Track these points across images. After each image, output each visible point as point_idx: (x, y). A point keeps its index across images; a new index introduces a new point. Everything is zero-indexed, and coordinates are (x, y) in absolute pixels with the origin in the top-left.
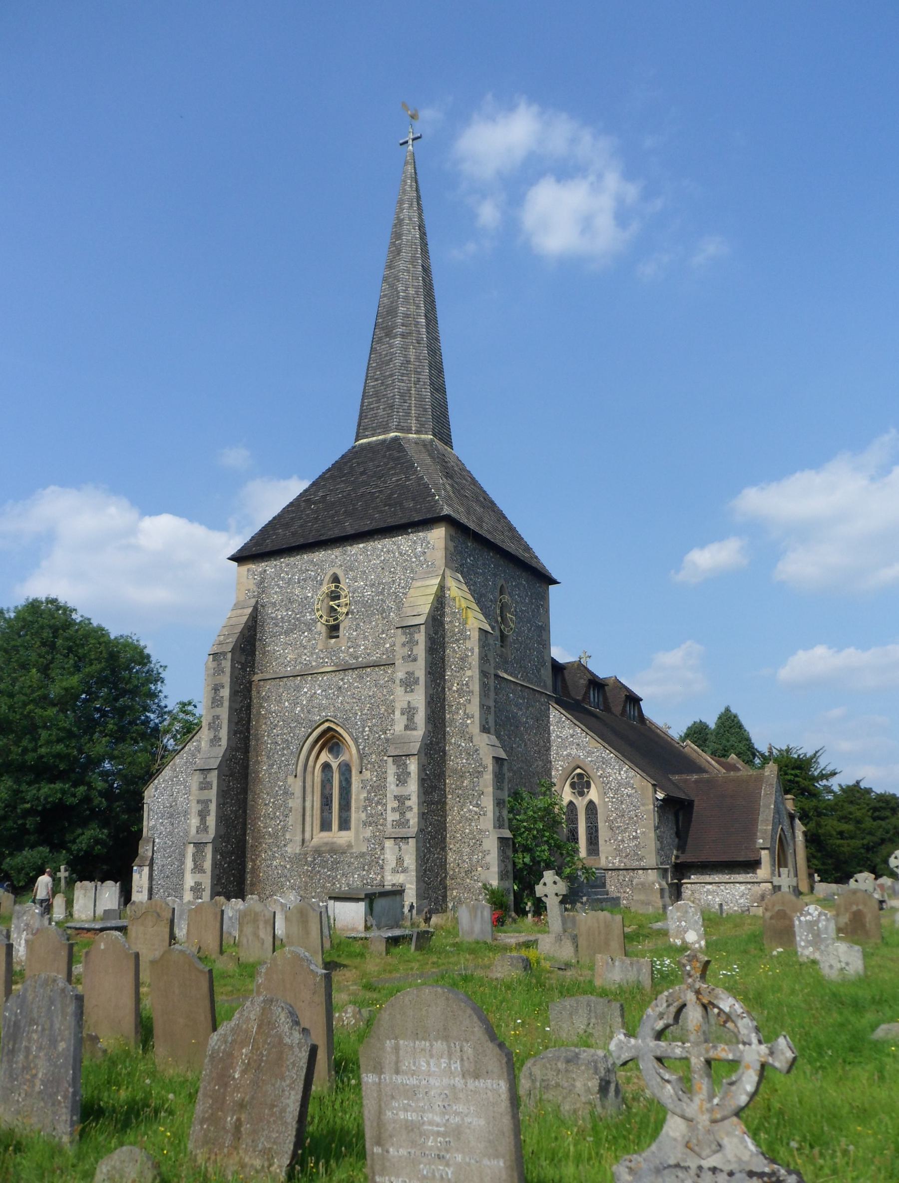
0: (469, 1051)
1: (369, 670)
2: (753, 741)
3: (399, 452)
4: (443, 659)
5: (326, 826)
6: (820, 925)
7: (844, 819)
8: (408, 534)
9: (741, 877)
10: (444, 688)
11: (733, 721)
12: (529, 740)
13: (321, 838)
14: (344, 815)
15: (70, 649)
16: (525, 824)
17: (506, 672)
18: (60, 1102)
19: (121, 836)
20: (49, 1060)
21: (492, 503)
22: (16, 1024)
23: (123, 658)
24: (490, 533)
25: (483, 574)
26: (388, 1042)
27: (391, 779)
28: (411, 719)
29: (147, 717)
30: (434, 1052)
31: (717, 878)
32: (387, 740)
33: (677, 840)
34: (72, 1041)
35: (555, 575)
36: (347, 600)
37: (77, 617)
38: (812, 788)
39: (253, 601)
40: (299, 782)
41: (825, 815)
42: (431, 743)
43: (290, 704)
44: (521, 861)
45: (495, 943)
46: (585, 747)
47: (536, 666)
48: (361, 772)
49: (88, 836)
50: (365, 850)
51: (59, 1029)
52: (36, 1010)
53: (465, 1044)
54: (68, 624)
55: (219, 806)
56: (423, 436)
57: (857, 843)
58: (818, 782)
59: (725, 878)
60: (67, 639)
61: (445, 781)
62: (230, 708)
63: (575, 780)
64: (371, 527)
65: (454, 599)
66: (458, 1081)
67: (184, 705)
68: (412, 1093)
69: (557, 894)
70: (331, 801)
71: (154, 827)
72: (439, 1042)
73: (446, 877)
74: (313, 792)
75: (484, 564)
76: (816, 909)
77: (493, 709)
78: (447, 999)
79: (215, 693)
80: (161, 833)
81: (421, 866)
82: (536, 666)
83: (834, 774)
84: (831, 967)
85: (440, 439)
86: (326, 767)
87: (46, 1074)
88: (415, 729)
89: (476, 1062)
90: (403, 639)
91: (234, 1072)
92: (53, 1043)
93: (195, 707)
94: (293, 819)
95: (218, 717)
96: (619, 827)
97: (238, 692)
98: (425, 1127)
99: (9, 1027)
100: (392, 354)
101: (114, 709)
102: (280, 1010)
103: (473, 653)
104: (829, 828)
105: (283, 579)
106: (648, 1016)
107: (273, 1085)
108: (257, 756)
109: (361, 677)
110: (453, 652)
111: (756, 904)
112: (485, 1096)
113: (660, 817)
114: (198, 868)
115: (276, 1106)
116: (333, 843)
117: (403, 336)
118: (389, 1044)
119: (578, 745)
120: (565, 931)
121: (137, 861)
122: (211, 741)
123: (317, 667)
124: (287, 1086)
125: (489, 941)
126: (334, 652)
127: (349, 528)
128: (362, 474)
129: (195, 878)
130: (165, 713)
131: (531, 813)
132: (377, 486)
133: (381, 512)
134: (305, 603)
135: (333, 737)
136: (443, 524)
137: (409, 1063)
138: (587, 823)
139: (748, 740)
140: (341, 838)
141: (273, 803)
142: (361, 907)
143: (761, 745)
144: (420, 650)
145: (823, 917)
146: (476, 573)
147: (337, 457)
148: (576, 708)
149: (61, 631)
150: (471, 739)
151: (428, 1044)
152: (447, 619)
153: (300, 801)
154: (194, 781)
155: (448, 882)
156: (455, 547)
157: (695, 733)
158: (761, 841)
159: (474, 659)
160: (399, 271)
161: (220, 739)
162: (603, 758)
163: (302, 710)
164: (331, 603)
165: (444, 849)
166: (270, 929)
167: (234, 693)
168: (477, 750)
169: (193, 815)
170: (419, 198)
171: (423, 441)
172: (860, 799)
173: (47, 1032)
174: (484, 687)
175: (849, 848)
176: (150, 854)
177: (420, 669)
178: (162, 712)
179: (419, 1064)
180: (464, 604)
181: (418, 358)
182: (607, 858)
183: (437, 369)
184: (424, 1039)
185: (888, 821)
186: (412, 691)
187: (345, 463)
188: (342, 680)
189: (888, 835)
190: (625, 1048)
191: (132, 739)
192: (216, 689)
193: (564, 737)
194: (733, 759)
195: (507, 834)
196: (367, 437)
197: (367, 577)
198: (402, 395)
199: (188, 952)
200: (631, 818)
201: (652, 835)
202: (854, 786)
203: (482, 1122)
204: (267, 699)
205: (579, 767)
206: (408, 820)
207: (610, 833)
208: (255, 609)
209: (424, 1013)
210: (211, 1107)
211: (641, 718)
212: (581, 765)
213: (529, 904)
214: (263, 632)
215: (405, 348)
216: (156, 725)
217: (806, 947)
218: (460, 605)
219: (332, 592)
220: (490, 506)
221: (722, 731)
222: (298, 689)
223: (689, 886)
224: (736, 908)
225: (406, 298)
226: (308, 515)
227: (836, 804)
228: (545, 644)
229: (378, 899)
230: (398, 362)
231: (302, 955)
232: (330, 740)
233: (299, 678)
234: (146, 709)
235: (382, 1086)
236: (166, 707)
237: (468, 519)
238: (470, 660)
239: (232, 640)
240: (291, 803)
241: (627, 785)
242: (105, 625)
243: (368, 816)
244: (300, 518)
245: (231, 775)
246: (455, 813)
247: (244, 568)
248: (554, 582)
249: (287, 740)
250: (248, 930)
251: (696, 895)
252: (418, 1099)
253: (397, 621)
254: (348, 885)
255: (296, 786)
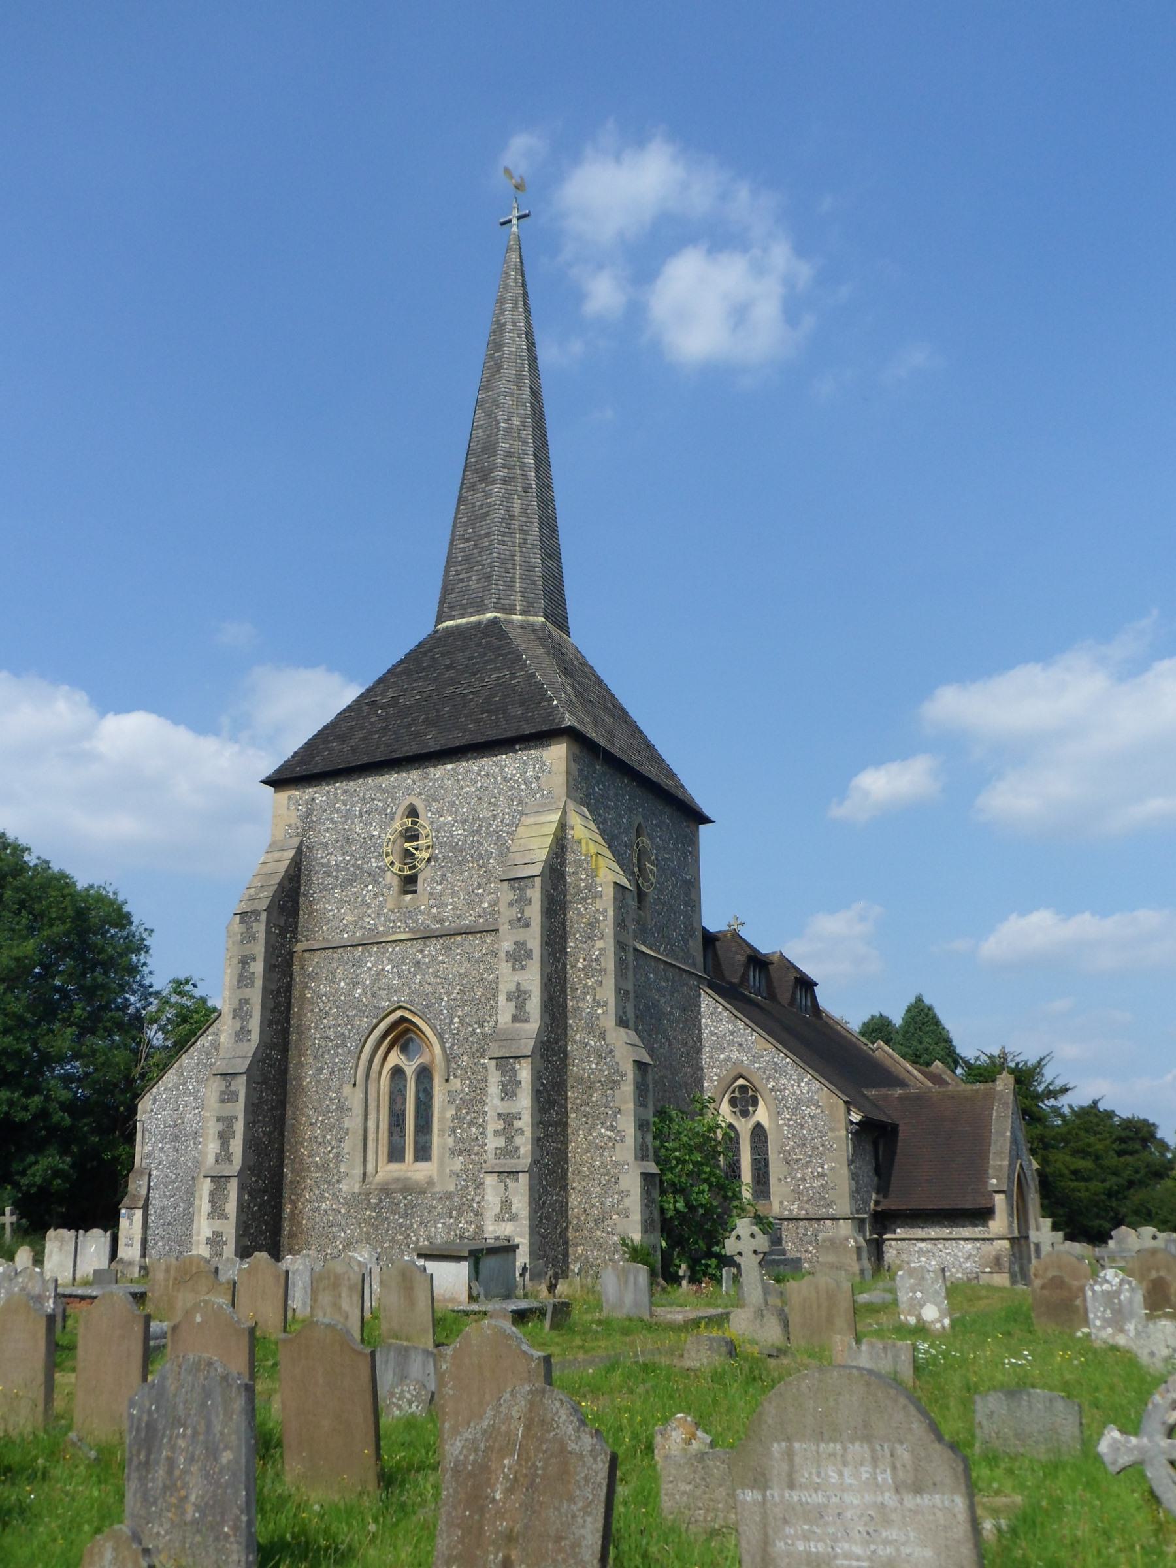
0: (904, 1454)
1: (459, 938)
2: (954, 1043)
3: (500, 639)
4: (564, 924)
5: (396, 1154)
6: (1122, 1297)
7: (1082, 1153)
8: (515, 752)
9: (966, 1232)
10: (565, 965)
11: (927, 1015)
12: (675, 1038)
13: (389, 1171)
14: (422, 1140)
15: (22, 904)
16: (677, 1154)
17: (644, 943)
18: (227, 1536)
19: (89, 1166)
20: (207, 1476)
21: (623, 710)
22: (151, 1427)
23: (94, 917)
24: (624, 752)
25: (616, 807)
26: (775, 1445)
27: (494, 1090)
28: (521, 1007)
29: (127, 1000)
30: (849, 1457)
31: (932, 1232)
32: (485, 1035)
33: (876, 1179)
34: (244, 1450)
35: (707, 811)
36: (429, 841)
37: (30, 859)
38: (1035, 1109)
39: (296, 841)
40: (359, 1094)
41: (1053, 1147)
42: (548, 1040)
43: (348, 984)
44: (671, 1206)
45: (654, 1320)
46: (750, 1048)
47: (683, 936)
48: (447, 1080)
49: (44, 1166)
50: (452, 1189)
51: (222, 1434)
52: (181, 1406)
53: (897, 1446)
54: (20, 868)
55: (249, 1125)
56: (531, 618)
57: (1096, 1186)
58: (1043, 1101)
59: (945, 1232)
60: (17, 890)
61: (566, 1093)
62: (264, 989)
63: (737, 1094)
64: (463, 742)
65: (579, 842)
66: (889, 1499)
67: (178, 983)
68: (817, 1515)
69: (755, 1252)
70: (404, 1120)
71: (150, 1154)
72: (857, 1444)
73: (567, 1228)
74: (378, 1106)
75: (616, 795)
76: (1116, 1275)
77: (632, 995)
78: (868, 1384)
79: (243, 968)
80: (160, 1163)
81: (536, 1212)
82: (683, 936)
83: (1064, 1090)
84: (1152, 1354)
85: (554, 623)
86: (397, 1072)
87: (203, 1497)
88: (527, 1021)
89: (916, 1470)
90: (511, 896)
91: (494, 1491)
92: (213, 1453)
93: (195, 986)
94: (351, 1144)
95: (247, 1001)
96: (798, 1160)
97: (275, 966)
98: (839, 1562)
99: (138, 1430)
100: (490, 505)
101: (81, 988)
102: (558, 1404)
103: (605, 917)
104: (1059, 1165)
105: (338, 811)
106: (1156, 1406)
107: (558, 1509)
108: (300, 1057)
109: (448, 948)
110: (578, 914)
111: (988, 1270)
112: (931, 1518)
113: (854, 1147)
114: (217, 1212)
115: (566, 1538)
116: (407, 1179)
117: (505, 481)
118: (777, 1448)
119: (740, 1045)
120: (767, 1304)
121: (126, 1201)
122: (237, 1034)
123: (386, 933)
124: (579, 1510)
125: (647, 1317)
126: (411, 913)
127: (432, 741)
128: (448, 668)
129: (210, 1227)
130: (151, 994)
131: (685, 1139)
132: (470, 685)
133: (477, 721)
134: (369, 844)
135: (407, 1030)
136: (565, 739)
137: (810, 1474)
138: (752, 1154)
139: (948, 1041)
140: (419, 1172)
141: (322, 1122)
142: (464, 1268)
143: (967, 1050)
144: (535, 912)
145: (1127, 1286)
146: (607, 807)
147: (411, 644)
148: (731, 993)
149: (10, 879)
150: (603, 1036)
151: (839, 1447)
152: (569, 869)
153: (359, 1119)
154: (212, 1091)
155: (570, 1235)
156: (580, 771)
157: (873, 1031)
158: (994, 1181)
159: (608, 926)
160: (499, 394)
161: (249, 1031)
162: (776, 1064)
163: (364, 993)
164: (407, 845)
165: (564, 1188)
166: (356, 1298)
167: (270, 968)
168: (611, 1051)
169: (211, 1137)
170: (525, 295)
171: (532, 625)
172: (1098, 1125)
173: (201, 1438)
174: (621, 963)
175: (1087, 1194)
176: (144, 1192)
177: (534, 939)
178: (147, 993)
179: (826, 1474)
180: (593, 849)
181: (524, 512)
182: (781, 1203)
183: (549, 526)
184: (834, 1441)
185: (1137, 1156)
186: (523, 968)
187: (425, 653)
188: (422, 951)
189: (1138, 1176)
190: (1123, 1449)
191: (105, 1029)
192: (245, 962)
193: (720, 1034)
194: (937, 1067)
195: (653, 1168)
196: (453, 618)
197: (457, 810)
198: (502, 562)
199: (340, 1326)
200: (815, 1148)
201: (845, 1171)
202: (1090, 1107)
203: (929, 1553)
204: (314, 976)
205: (741, 1076)
206: (518, 1148)
207: (785, 1168)
208: (299, 851)
209: (832, 1403)
210: (461, 1541)
211: (816, 1009)
212: (745, 1074)
213: (684, 1266)
214: (310, 884)
215: (507, 498)
216: (138, 1010)
217: (1103, 1328)
218: (588, 850)
219: (407, 830)
220: (621, 714)
221: (912, 1029)
222: (359, 963)
223: (893, 1243)
224: (960, 1275)
225: (509, 431)
226: (372, 723)
227: (1069, 1133)
228: (693, 905)
229: (484, 1257)
230: (497, 516)
231: (508, 1331)
232: (402, 1034)
233: (360, 948)
234: (122, 988)
235: (769, 1505)
236: (151, 986)
237: (596, 732)
238: (602, 926)
239: (268, 894)
240: (347, 1123)
241: (810, 1102)
242: (69, 871)
243: (457, 1142)
244: (362, 728)
245: (264, 1083)
246: (580, 1141)
247: (284, 796)
248: (706, 820)
249: (343, 1034)
250: (325, 1299)
251: (904, 1256)
252: (827, 1524)
253: (500, 872)
254: (428, 1237)
255: (354, 1099)
